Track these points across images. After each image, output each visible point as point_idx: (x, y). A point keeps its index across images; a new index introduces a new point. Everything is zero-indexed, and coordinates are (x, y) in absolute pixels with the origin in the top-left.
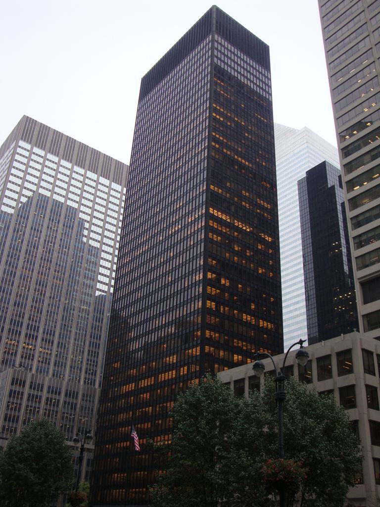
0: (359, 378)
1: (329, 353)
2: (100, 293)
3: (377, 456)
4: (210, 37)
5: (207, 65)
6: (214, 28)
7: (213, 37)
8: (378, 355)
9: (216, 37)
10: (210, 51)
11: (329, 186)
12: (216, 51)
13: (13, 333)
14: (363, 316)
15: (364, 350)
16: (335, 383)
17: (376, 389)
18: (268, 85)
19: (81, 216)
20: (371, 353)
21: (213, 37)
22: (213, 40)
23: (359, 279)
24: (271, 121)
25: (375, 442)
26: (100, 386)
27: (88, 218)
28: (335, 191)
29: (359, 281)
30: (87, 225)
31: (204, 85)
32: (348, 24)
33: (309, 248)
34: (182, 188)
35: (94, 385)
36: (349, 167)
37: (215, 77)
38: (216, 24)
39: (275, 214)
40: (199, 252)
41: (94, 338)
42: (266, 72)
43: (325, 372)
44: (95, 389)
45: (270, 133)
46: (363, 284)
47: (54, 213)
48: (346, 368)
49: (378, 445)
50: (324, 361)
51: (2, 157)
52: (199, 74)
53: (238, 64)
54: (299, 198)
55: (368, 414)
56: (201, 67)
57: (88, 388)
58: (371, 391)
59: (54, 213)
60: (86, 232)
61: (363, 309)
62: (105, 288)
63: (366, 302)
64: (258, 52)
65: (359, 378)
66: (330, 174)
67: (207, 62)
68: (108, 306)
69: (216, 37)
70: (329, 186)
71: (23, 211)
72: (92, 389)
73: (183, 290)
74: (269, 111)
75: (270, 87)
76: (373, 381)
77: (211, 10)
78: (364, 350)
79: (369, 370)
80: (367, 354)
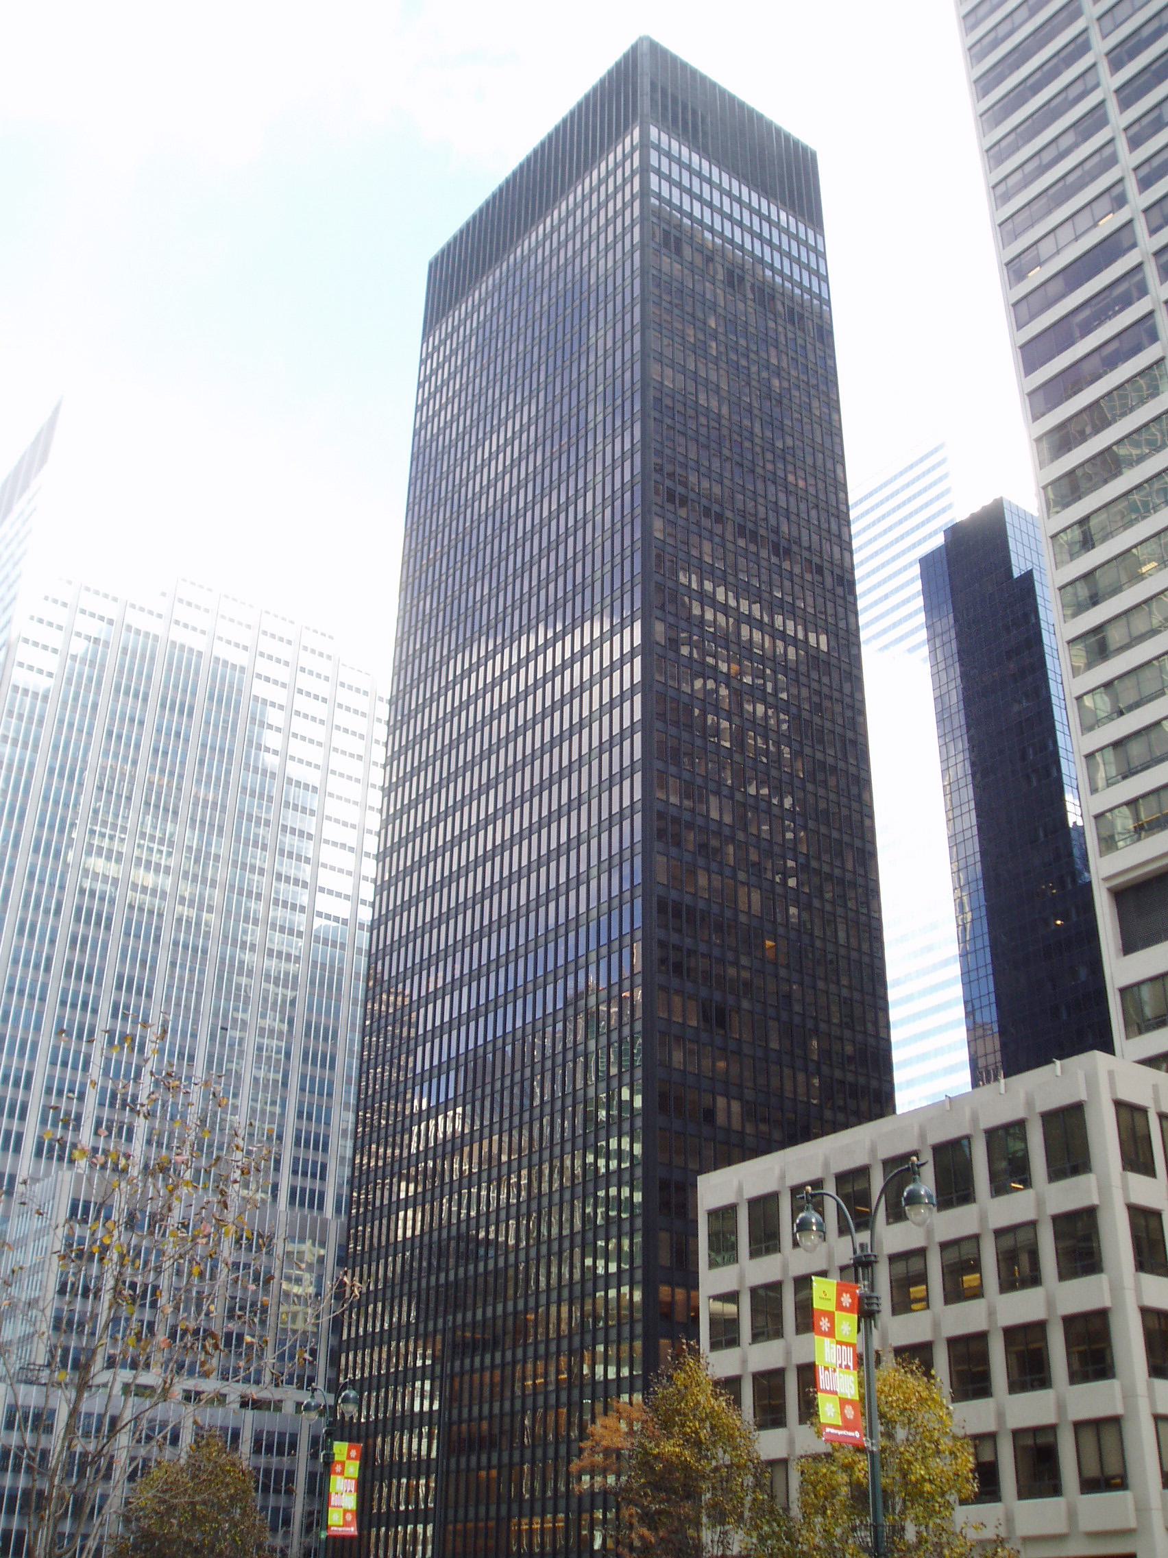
0: (1110, 1188)
1: (1019, 1114)
2: (325, 922)
3: (1164, 1409)
4: (636, 132)
5: (628, 222)
6: (645, 104)
7: (644, 135)
8: (1162, 1116)
9: (653, 131)
10: (637, 155)
11: (1016, 574)
12: (654, 179)
13: (99, 916)
14: (1123, 991)
15: (1119, 1105)
16: (1040, 1203)
17: (1157, 1214)
18: (817, 273)
19: (260, 689)
20: (1143, 1111)
21: (644, 135)
22: (645, 145)
23: (1106, 879)
24: (857, 695)
25: (1157, 1370)
26: (338, 1210)
27: (279, 696)
28: (1048, 688)
29: (1108, 885)
30: (274, 717)
31: (615, 242)
32: (1094, 205)
33: (983, 981)
34: (569, 605)
35: (321, 1207)
36: (1068, 489)
37: (664, 786)
38: (649, 94)
39: (880, 1002)
40: (616, 809)
41: (312, 1092)
42: (811, 233)
43: (1012, 1173)
44: (325, 1223)
45: (839, 536)
46: (1120, 895)
47: (134, 959)
48: (1070, 1155)
49: (1153, 1270)
50: (1006, 1138)
51: (5, 517)
52: (607, 225)
53: (721, 206)
54: (967, 1014)
55: (1125, 1188)
56: (602, 213)
57: (304, 1219)
58: (1145, 1221)
59: (134, 959)
60: (271, 739)
61: (1121, 969)
62: (342, 909)
63: (1129, 946)
64: (787, 176)
65: (1110, 1188)
66: (1020, 552)
67: (628, 188)
68: (353, 988)
69: (653, 131)
70: (1016, 574)
71: (82, 681)
72: (314, 1220)
73: (574, 843)
74: (854, 743)
75: (821, 255)
76: (1145, 1191)
77: (634, 49)
78: (1119, 1105)
79: (1137, 1158)
80: (1130, 1114)
